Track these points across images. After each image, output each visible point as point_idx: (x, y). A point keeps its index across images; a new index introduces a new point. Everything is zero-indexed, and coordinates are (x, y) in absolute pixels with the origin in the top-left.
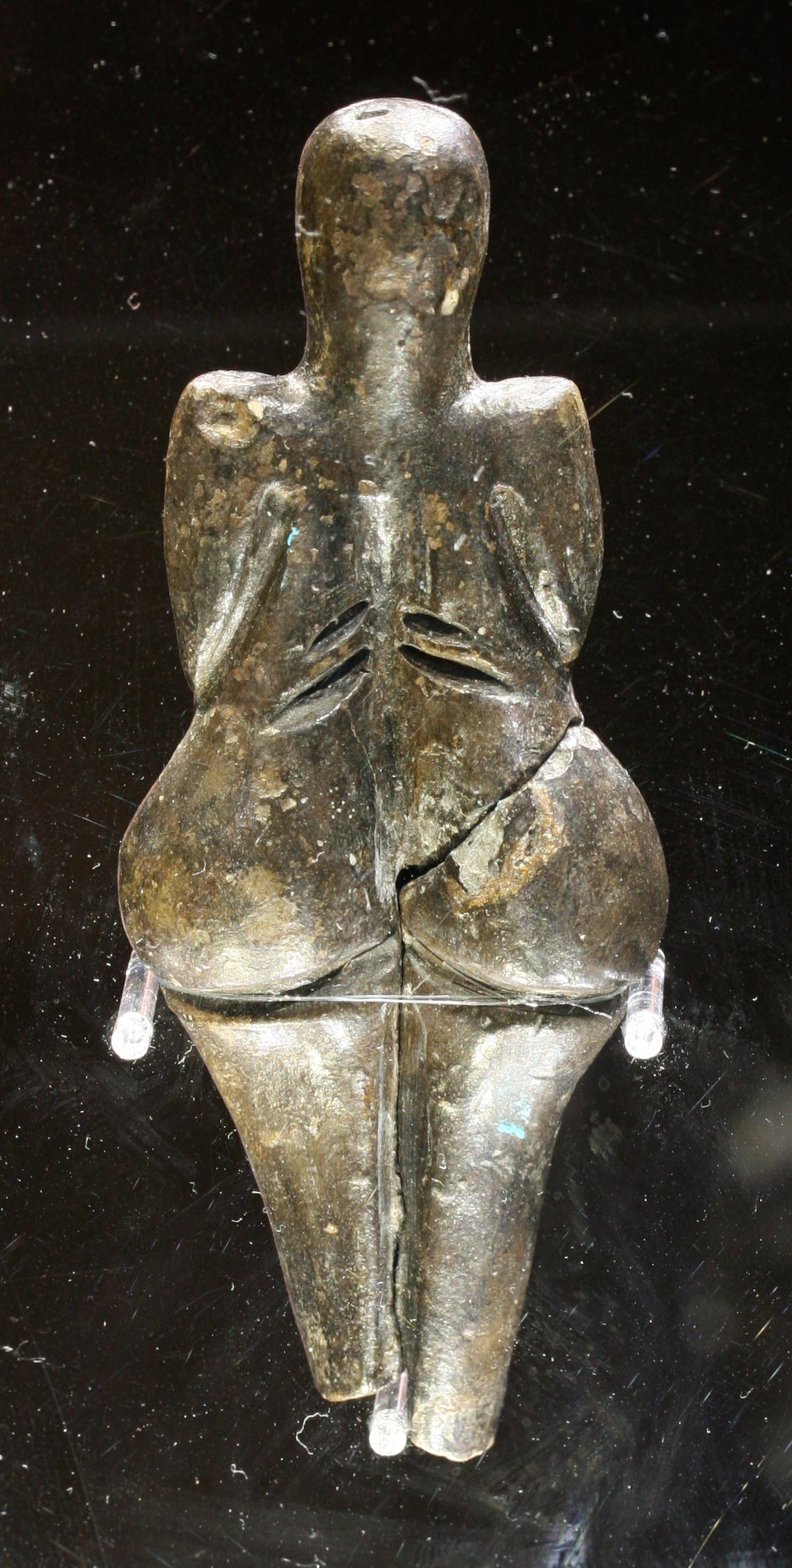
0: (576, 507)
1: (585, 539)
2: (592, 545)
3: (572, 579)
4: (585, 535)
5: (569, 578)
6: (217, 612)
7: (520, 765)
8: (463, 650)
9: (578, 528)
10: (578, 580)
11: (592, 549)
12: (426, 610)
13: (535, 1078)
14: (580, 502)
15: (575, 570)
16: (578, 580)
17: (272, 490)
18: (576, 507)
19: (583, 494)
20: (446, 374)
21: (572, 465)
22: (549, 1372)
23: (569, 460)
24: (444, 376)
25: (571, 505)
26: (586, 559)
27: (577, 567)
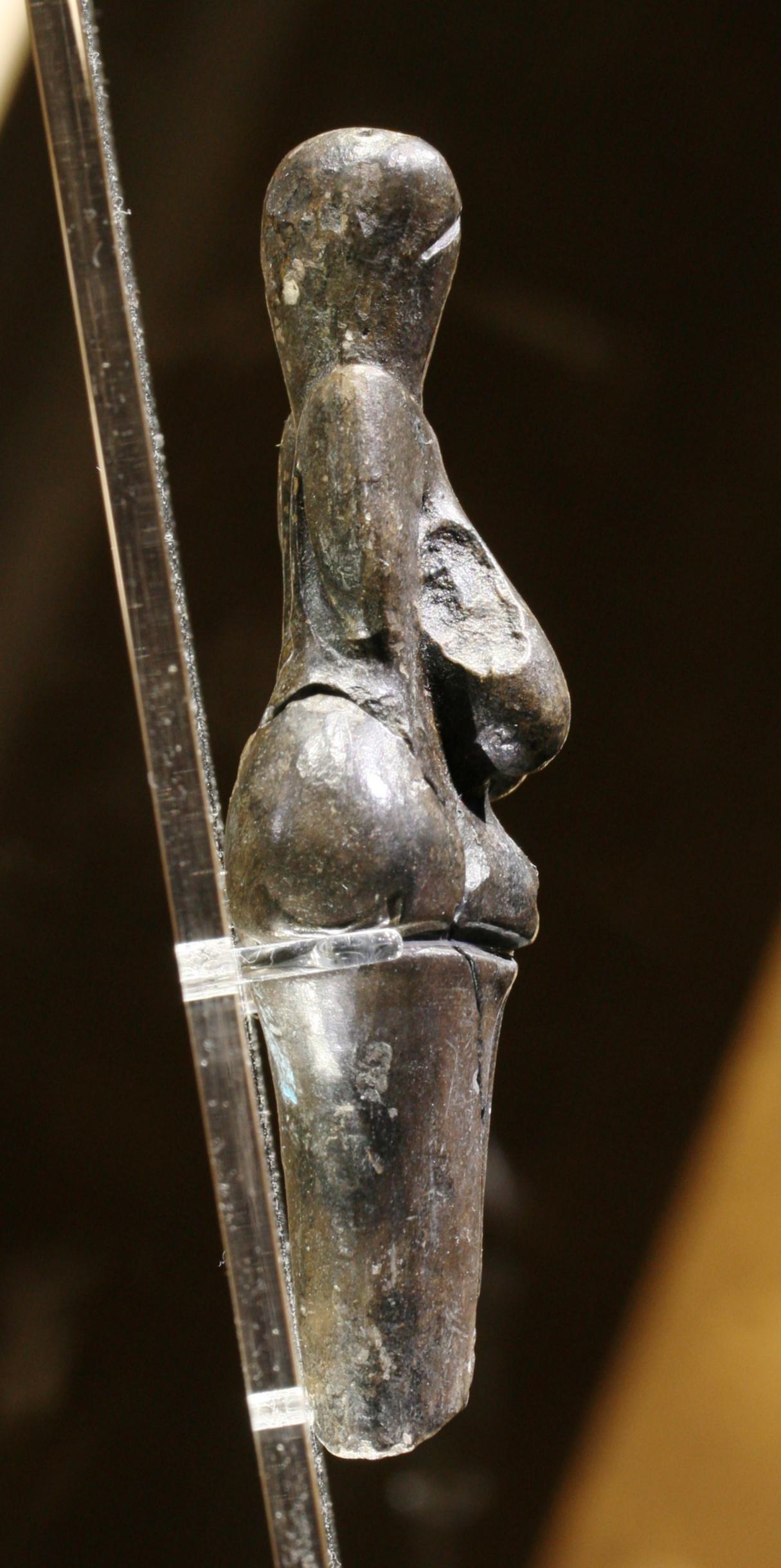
0: (325, 479)
1: (333, 511)
2: (341, 518)
3: (324, 549)
4: (332, 506)
5: (321, 548)
6: (292, 377)
7: (132, 301)
8: (226, 987)
9: (326, 498)
10: (328, 550)
11: (341, 522)
12: (282, 530)
13: (346, 696)
14: (329, 474)
15: (326, 541)
16: (328, 550)
17: (244, 977)
18: (325, 479)
19: (332, 467)
20: (311, 365)
21: (326, 439)
22: (335, 911)
23: (324, 433)
24: (310, 366)
25: (322, 476)
26: (336, 531)
27: (327, 537)
